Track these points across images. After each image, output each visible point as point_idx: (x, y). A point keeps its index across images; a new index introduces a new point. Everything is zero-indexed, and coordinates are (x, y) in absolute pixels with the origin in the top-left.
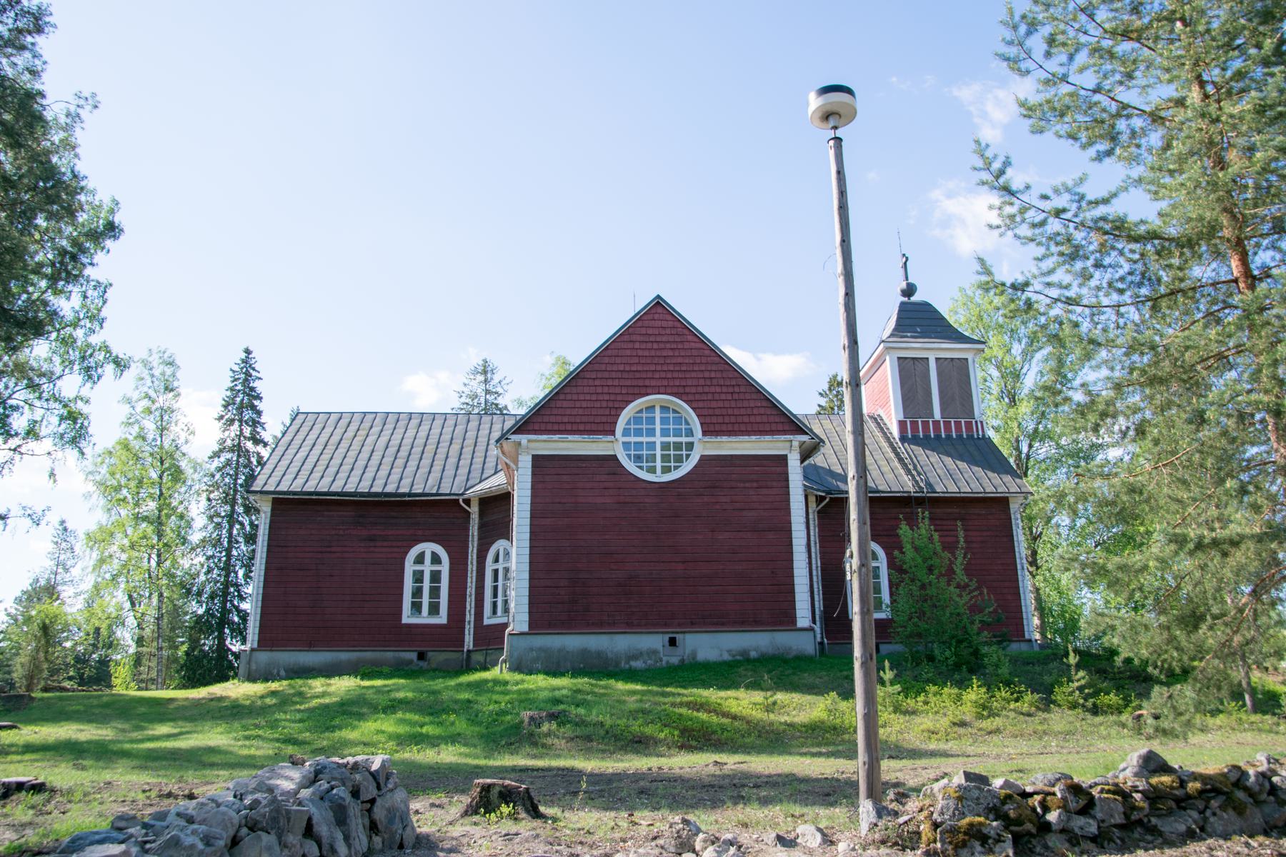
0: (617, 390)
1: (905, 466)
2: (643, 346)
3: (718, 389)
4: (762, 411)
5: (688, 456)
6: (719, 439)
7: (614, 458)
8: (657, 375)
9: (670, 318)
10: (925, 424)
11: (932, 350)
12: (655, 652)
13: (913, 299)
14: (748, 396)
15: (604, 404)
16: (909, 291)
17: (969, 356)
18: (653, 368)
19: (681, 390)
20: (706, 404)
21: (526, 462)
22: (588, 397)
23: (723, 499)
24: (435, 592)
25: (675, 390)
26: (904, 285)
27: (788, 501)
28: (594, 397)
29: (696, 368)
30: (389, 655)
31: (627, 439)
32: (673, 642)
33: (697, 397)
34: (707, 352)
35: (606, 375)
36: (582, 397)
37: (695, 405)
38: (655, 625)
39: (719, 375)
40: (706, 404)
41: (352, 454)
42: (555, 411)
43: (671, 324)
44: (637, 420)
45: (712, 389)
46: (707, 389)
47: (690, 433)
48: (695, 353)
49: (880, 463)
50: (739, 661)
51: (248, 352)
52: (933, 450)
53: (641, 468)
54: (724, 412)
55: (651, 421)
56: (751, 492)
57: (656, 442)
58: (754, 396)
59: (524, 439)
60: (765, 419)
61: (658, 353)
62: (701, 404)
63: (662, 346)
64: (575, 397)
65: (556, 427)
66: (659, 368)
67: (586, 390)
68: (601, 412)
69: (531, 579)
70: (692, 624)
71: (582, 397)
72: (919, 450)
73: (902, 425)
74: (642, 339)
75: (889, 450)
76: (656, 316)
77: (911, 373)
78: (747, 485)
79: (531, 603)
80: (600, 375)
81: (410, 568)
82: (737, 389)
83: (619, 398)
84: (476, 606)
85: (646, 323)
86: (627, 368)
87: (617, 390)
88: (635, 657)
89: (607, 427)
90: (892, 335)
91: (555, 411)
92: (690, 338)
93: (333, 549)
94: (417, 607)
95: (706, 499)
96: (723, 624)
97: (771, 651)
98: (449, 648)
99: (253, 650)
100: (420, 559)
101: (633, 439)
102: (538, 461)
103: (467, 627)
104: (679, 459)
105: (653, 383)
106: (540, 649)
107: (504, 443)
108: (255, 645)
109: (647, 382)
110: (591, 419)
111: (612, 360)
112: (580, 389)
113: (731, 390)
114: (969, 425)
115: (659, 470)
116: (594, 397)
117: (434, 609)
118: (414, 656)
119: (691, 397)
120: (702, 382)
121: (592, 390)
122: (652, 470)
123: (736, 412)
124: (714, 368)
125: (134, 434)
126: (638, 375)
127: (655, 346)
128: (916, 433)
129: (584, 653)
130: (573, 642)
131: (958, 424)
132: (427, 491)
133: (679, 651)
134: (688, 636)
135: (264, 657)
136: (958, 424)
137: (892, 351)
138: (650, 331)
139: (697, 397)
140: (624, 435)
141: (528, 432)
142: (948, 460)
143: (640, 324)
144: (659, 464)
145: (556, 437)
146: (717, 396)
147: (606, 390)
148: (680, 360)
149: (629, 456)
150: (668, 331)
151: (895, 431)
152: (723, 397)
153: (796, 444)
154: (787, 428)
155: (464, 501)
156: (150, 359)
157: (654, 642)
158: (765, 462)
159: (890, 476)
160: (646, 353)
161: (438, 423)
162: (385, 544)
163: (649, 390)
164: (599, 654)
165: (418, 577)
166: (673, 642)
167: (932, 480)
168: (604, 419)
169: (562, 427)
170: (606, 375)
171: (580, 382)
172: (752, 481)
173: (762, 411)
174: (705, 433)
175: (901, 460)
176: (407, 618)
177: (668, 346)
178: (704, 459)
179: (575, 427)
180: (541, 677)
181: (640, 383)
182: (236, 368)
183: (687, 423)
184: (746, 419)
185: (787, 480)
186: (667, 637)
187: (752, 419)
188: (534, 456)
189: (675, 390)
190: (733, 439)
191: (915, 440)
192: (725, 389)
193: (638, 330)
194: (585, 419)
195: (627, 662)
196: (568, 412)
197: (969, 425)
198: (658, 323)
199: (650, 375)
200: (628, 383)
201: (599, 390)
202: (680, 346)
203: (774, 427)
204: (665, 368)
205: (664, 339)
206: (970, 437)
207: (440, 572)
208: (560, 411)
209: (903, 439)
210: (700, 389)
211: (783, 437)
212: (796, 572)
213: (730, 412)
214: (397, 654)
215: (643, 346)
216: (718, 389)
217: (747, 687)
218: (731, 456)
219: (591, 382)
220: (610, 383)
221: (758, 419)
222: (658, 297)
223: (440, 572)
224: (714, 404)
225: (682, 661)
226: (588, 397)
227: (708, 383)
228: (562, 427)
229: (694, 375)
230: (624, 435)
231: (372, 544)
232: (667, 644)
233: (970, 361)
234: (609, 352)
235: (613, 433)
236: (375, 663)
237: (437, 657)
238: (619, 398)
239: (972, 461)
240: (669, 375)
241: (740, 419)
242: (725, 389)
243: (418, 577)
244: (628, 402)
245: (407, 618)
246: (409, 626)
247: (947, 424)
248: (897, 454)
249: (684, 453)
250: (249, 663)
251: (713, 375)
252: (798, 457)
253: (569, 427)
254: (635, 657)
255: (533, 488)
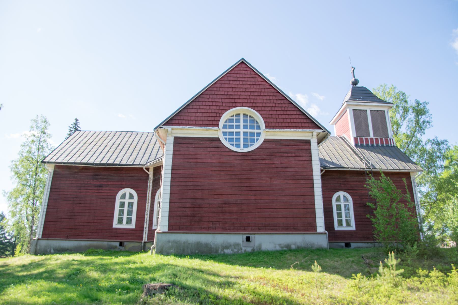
0: (221, 104)
1: (359, 157)
2: (235, 83)
3: (274, 105)
4: (297, 116)
5: (257, 139)
6: (274, 130)
7: (218, 139)
8: (241, 97)
9: (249, 69)
10: (367, 139)
11: (369, 107)
12: (238, 245)
13: (357, 86)
14: (289, 109)
15: (213, 111)
16: (355, 83)
17: (385, 109)
18: (239, 93)
19: (254, 105)
20: (267, 112)
21: (171, 141)
22: (205, 107)
23: (277, 162)
24: (130, 213)
25: (251, 105)
26: (353, 80)
27: (311, 164)
28: (208, 107)
29: (262, 94)
30: (105, 243)
31: (225, 130)
32: (248, 239)
33: (263, 108)
34: (268, 87)
35: (215, 96)
36: (201, 107)
37: (262, 112)
38: (238, 230)
39: (274, 98)
40: (267, 112)
41: (96, 147)
42: (187, 114)
43: (249, 72)
44: (231, 120)
45: (271, 105)
46: (268, 105)
47: (258, 127)
48: (261, 87)
49: (347, 156)
50: (285, 251)
51: (77, 120)
52: (372, 151)
53: (233, 145)
54: (277, 116)
55: (238, 121)
56: (291, 159)
57: (242, 132)
58: (293, 109)
59: (169, 128)
60: (298, 120)
61: (242, 86)
62: (265, 112)
63: (244, 83)
64: (198, 107)
65: (187, 122)
66: (243, 94)
67: (204, 104)
68: (211, 115)
69: (171, 202)
70: (259, 229)
71: (201, 107)
72: (365, 151)
73: (356, 139)
74: (234, 79)
75: (351, 150)
76: (242, 69)
77: (359, 117)
78: (289, 155)
79: (170, 216)
80: (211, 96)
81: (118, 200)
82: (284, 105)
83: (221, 108)
84: (150, 220)
85: (236, 72)
86: (226, 93)
87: (221, 104)
88: (227, 247)
89: (214, 123)
90: (350, 99)
91: (187, 114)
92: (259, 79)
93: (82, 191)
94: (120, 221)
95: (267, 162)
96: (276, 230)
97: (303, 245)
98: (134, 240)
99: (38, 239)
100: (123, 196)
101: (228, 130)
102: (177, 140)
103: (145, 230)
104: (253, 141)
105: (239, 101)
106: (174, 242)
107: (160, 130)
108: (40, 237)
109: (236, 101)
110: (206, 118)
111: (218, 89)
112: (200, 103)
113: (280, 105)
114: (387, 140)
115: (242, 146)
116: (208, 107)
117: (129, 221)
118: (117, 244)
119: (259, 109)
120: (265, 101)
121: (207, 104)
122: (238, 146)
123: (283, 117)
124: (272, 94)
125: (27, 150)
126: (231, 97)
127: (241, 83)
128: (362, 143)
129: (199, 244)
130: (192, 238)
131: (382, 140)
132: (128, 163)
133: (251, 244)
134: (257, 236)
135: (44, 243)
136: (382, 140)
137: (350, 106)
138: (238, 76)
139: (263, 108)
140: (223, 128)
141: (172, 124)
142: (380, 156)
143: (233, 72)
144: (242, 143)
145: (187, 127)
146: (273, 109)
147: (214, 104)
148: (254, 90)
149: (226, 139)
150: (248, 76)
151: (352, 143)
152: (276, 109)
153: (315, 134)
154: (310, 125)
155: (146, 168)
156: (38, 120)
157: (237, 239)
158: (299, 143)
159: (353, 161)
160: (236, 86)
161: (140, 135)
162: (107, 188)
163: (237, 105)
164: (207, 245)
165: (122, 205)
166: (248, 239)
167: (373, 164)
168: (213, 119)
169: (190, 122)
170: (215, 96)
171: (201, 100)
172: (292, 153)
173: (297, 116)
174: (267, 127)
175: (357, 155)
176: (115, 225)
177: (248, 83)
178: (266, 141)
179: (197, 123)
180: (173, 257)
181: (233, 101)
182: (72, 126)
183: (257, 122)
184: (289, 120)
185: (311, 153)
186: (245, 237)
187: (292, 121)
188: (175, 137)
189: (251, 105)
190: (282, 130)
191: (362, 146)
192: (277, 105)
193: (232, 75)
194: (203, 118)
195: (222, 250)
196: (194, 114)
197: (387, 140)
198: (243, 72)
199: (238, 97)
200: (226, 100)
201: (211, 104)
202: (254, 83)
203: (303, 125)
204: (246, 94)
205: (246, 79)
206: (388, 146)
207: (133, 203)
208: (190, 114)
209: (357, 146)
210: (264, 105)
211: (308, 130)
212: (316, 202)
213: (280, 116)
214: (109, 243)
215: (235, 83)
216: (274, 105)
217: (294, 267)
218: (281, 139)
219: (206, 100)
220: (217, 100)
221: (295, 120)
222: (243, 59)
223: (133, 203)
224: (271, 112)
225: (253, 250)
226: (205, 107)
227: (269, 101)
228: (190, 122)
229: (261, 97)
230: (223, 128)
231: (101, 188)
232: (245, 240)
233: (386, 112)
234: (216, 85)
235: (217, 125)
236: (98, 247)
237: (129, 245)
238: (221, 108)
239: (391, 157)
240: (248, 97)
241: (285, 120)
242: (277, 105)
243: (122, 205)
244: (226, 110)
245: (115, 225)
246: (116, 229)
247: (377, 140)
248: (355, 152)
249: (255, 138)
250: (36, 245)
251: (271, 98)
252: (316, 141)
253: (194, 122)
254: (227, 247)
255: (174, 154)
